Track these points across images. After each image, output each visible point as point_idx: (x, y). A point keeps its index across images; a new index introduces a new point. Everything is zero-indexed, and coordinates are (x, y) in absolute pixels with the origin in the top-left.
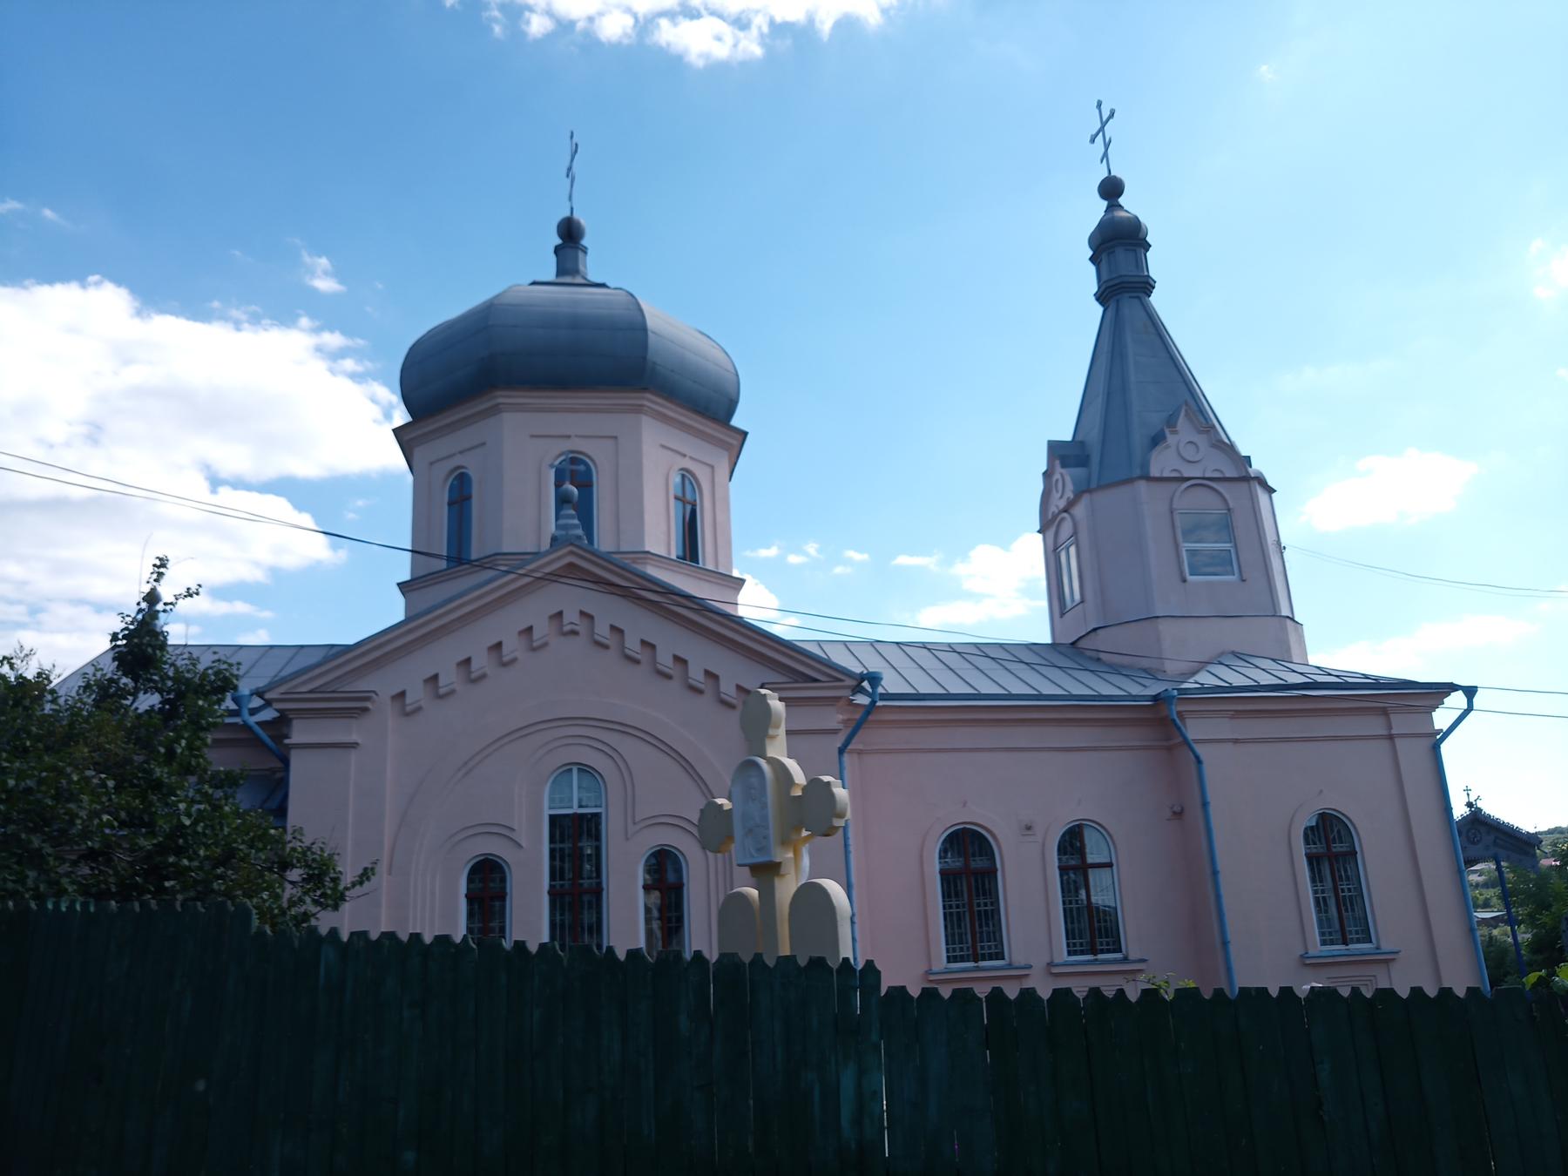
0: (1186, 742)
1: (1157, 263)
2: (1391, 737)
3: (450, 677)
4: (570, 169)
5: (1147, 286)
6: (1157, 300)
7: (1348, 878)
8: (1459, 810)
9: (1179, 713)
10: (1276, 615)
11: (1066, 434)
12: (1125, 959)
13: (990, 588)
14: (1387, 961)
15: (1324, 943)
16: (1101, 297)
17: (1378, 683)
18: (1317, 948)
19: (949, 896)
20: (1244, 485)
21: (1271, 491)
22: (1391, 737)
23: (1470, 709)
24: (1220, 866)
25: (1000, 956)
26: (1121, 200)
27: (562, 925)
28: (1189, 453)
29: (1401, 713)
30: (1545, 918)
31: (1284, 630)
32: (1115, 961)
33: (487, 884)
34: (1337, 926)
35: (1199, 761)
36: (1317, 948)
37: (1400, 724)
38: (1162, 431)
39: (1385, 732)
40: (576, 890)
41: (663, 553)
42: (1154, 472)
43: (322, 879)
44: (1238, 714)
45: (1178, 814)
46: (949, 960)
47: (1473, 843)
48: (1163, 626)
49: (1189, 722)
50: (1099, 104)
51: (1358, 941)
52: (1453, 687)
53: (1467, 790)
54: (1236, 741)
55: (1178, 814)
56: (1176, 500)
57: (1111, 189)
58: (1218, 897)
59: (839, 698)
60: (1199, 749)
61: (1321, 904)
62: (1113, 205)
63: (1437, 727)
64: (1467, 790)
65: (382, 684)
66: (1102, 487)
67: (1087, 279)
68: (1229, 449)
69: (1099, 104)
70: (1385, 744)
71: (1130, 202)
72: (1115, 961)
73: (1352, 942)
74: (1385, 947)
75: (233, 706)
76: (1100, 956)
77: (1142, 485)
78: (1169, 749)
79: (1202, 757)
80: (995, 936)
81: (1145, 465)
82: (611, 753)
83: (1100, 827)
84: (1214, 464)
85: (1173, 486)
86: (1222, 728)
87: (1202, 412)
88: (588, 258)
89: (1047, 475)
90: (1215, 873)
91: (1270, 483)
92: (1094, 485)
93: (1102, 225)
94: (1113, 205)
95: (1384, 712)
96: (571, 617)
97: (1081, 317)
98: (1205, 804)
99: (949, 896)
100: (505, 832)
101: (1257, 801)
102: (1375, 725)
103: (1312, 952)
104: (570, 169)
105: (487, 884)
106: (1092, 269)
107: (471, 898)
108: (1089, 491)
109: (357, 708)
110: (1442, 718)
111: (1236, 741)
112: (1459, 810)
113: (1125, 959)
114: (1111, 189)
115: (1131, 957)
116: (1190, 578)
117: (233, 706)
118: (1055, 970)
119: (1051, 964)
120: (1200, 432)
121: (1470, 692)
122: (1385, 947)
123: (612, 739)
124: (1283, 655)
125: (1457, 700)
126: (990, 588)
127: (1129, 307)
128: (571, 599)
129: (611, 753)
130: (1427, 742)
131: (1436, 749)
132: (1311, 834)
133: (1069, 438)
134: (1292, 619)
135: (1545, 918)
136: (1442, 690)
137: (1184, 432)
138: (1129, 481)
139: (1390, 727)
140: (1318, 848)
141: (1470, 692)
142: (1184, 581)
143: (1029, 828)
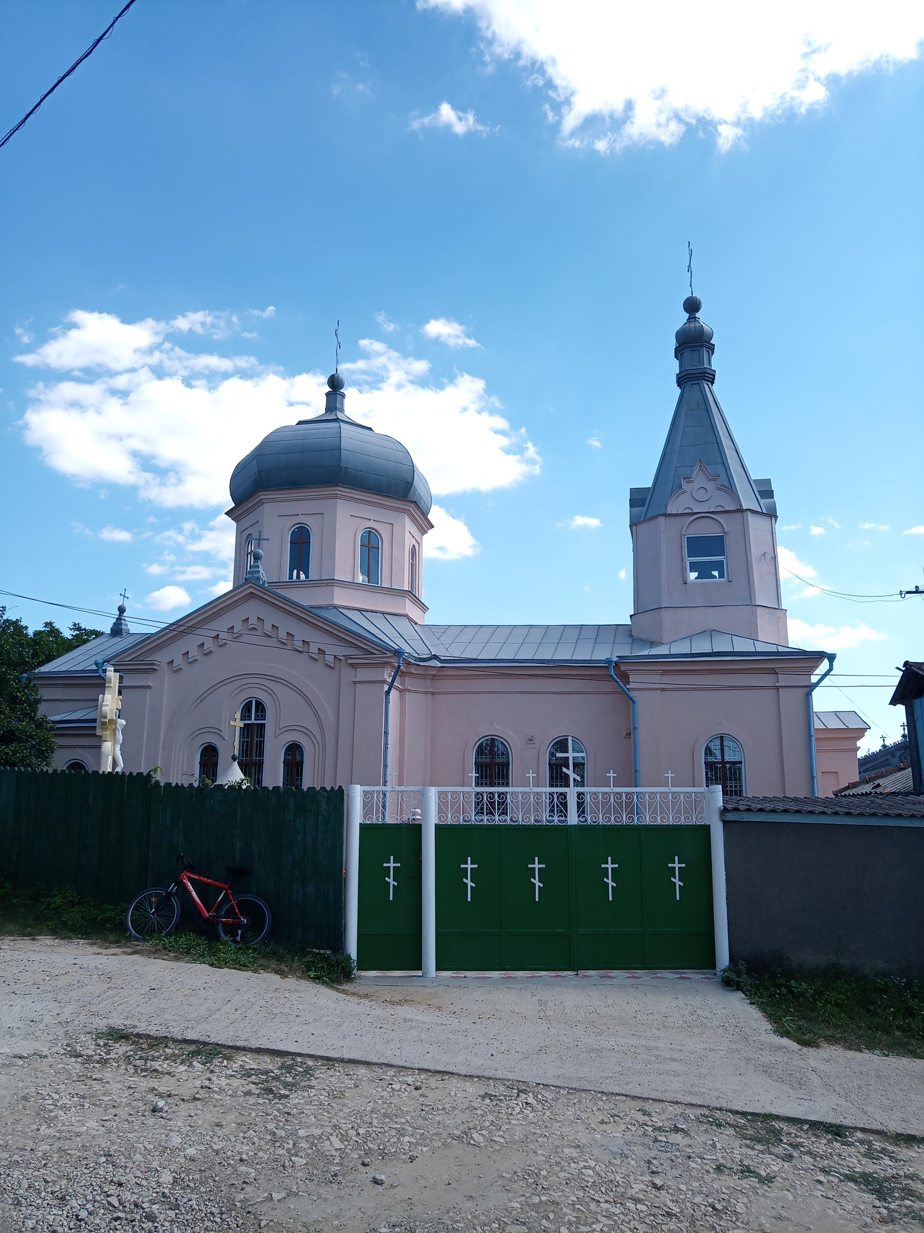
3: (194, 653)
4: (689, 266)
5: (711, 378)
7: (736, 779)
11: (648, 483)
20: (740, 515)
26: (698, 315)
27: (731, 780)
28: (700, 496)
33: (210, 759)
40: (251, 762)
41: (348, 579)
43: (904, 736)
44: (665, 672)
48: (665, 614)
54: (663, 690)
57: (692, 306)
59: (386, 663)
62: (692, 318)
65: (161, 658)
70: (774, 692)
77: (662, 519)
82: (271, 693)
83: (734, 739)
88: (346, 400)
94: (692, 318)
96: (253, 621)
100: (218, 732)
102: (768, 680)
104: (689, 266)
105: (210, 759)
107: (201, 763)
109: (150, 669)
111: (663, 690)
114: (692, 306)
123: (270, 684)
125: (825, 665)
128: (253, 610)
129: (271, 693)
131: (809, 694)
132: (480, 751)
136: (819, 656)
138: (655, 517)
140: (485, 759)
141: (831, 658)
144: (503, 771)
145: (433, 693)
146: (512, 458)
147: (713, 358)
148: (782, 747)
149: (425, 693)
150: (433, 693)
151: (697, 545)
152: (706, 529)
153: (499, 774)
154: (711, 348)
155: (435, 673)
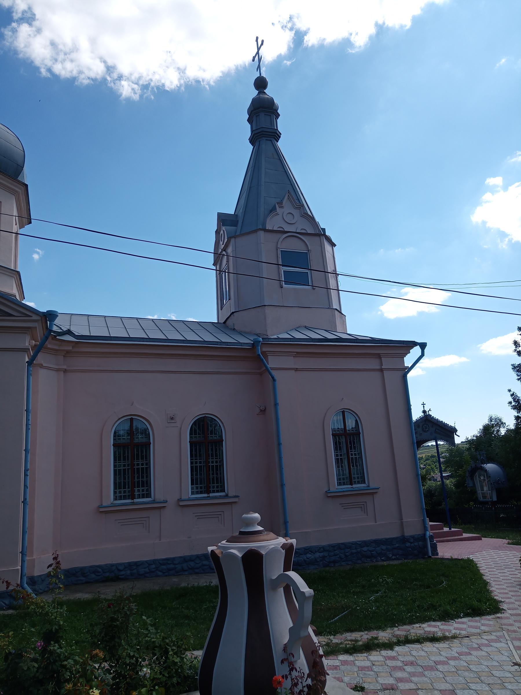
0: (267, 369)
1: (282, 124)
2: (381, 370)
5: (276, 136)
6: (281, 144)
8: (416, 414)
9: (263, 353)
10: (329, 307)
11: (231, 211)
12: (227, 496)
13: (187, 297)
14: (373, 494)
15: (339, 484)
16: (252, 141)
17: (373, 340)
18: (335, 487)
19: (120, 460)
20: (317, 239)
21: (333, 245)
22: (381, 370)
23: (423, 355)
24: (282, 441)
25: (148, 495)
28: (289, 219)
29: (389, 356)
30: (460, 472)
31: (334, 316)
32: (220, 497)
34: (348, 475)
35: (274, 380)
36: (335, 487)
37: (387, 363)
38: (275, 206)
39: (378, 367)
42: (268, 227)
44: (298, 355)
45: (263, 411)
46: (115, 499)
47: (425, 431)
48: (268, 310)
49: (270, 358)
50: (257, 38)
51: (359, 483)
52: (413, 344)
53: (423, 404)
54: (296, 370)
55: (263, 411)
56: (279, 243)
58: (280, 458)
60: (274, 373)
61: (339, 462)
63: (406, 365)
64: (423, 404)
66: (242, 235)
67: (246, 130)
68: (311, 219)
69: (257, 38)
70: (378, 374)
71: (269, 91)
72: (220, 497)
73: (355, 483)
74: (372, 485)
75: (97, 667)
76: (211, 495)
77: (262, 233)
78: (261, 374)
79: (276, 377)
80: (147, 484)
81: (264, 224)
84: (301, 226)
85: (279, 235)
86: (290, 362)
87: (299, 200)
89: (217, 232)
90: (279, 444)
91: (334, 241)
92: (238, 233)
93: (254, 100)
95: (379, 356)
97: (241, 151)
98: (276, 405)
99: (120, 460)
101: (308, 405)
102: (374, 364)
103: (332, 489)
106: (249, 126)
108: (235, 237)
110: (408, 361)
111: (296, 370)
112: (416, 414)
113: (227, 496)
115: (229, 495)
116: (284, 285)
117: (97, 667)
118: (182, 503)
119: (180, 500)
120: (296, 208)
121: (423, 346)
122: (372, 485)
124: (332, 329)
125: (416, 351)
126: (187, 297)
127: (265, 145)
130: (400, 373)
133: (232, 212)
134: (340, 312)
135: (460, 472)
136: (409, 345)
137: (287, 207)
138: (255, 231)
139: (382, 365)
141: (423, 346)
142: (282, 287)
143: (172, 419)
144: (142, 452)
145: (65, 371)
146: (303, 28)
147: (278, 120)
148: (101, 463)
149: (58, 370)
150: (65, 371)
151: (289, 258)
152: (294, 246)
153: (138, 455)
154: (278, 116)
155: (70, 348)
